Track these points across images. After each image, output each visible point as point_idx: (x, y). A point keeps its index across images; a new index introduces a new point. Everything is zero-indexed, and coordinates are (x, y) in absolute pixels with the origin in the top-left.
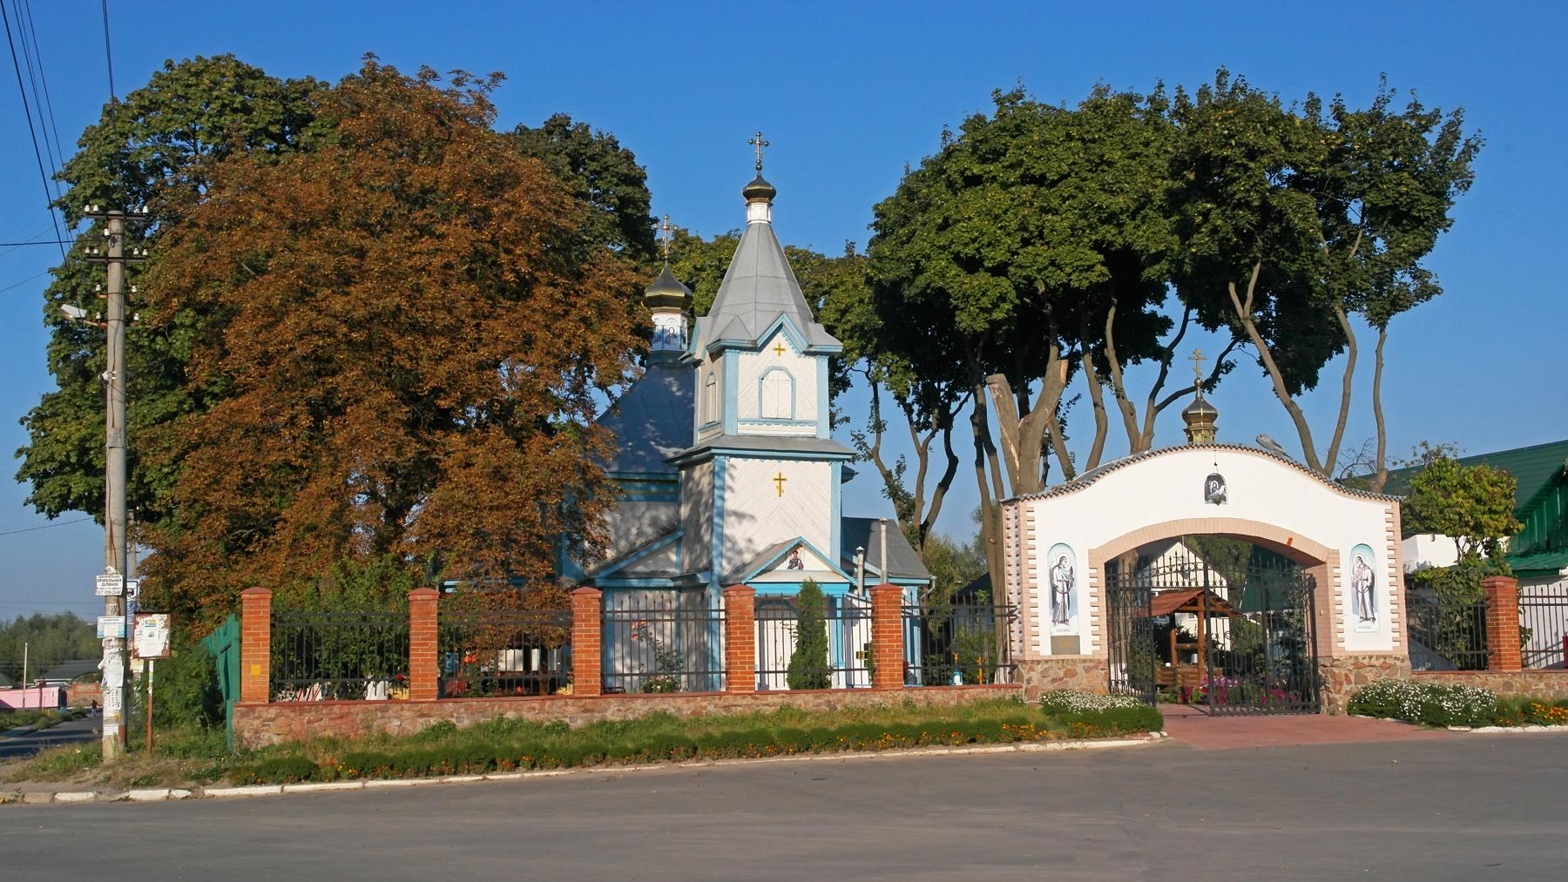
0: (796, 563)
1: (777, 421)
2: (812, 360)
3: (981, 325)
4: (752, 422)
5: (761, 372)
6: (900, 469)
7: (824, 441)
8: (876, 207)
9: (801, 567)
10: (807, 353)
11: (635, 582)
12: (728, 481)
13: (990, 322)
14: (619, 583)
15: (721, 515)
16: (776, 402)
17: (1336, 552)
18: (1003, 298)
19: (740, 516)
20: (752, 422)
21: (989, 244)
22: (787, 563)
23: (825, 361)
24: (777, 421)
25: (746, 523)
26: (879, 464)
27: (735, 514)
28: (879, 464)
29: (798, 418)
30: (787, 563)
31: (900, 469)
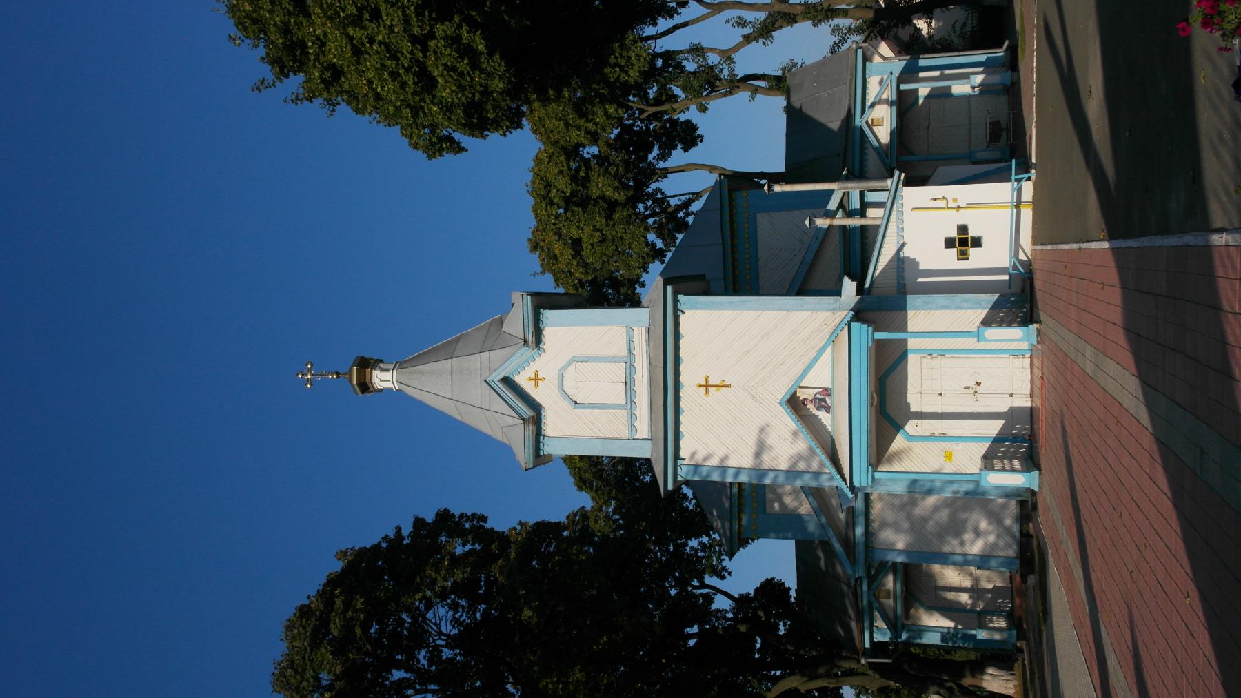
0: (821, 402)
1: (629, 383)
2: (548, 333)
3: (496, 64)
4: (632, 417)
5: (568, 405)
6: (742, 23)
7: (652, 316)
8: (430, 157)
9: (827, 392)
10: (538, 340)
11: (859, 531)
12: (714, 462)
13: (490, 55)
14: (860, 549)
15: (762, 473)
16: (604, 384)
17: (967, 259)
18: (454, 41)
19: (761, 448)
20: (632, 417)
21: (394, 57)
22: (822, 415)
23: (548, 315)
24: (629, 383)
25: (771, 440)
26: (736, 48)
27: (758, 455)
28: (736, 48)
29: (624, 353)
30: (822, 415)
31: (742, 23)
